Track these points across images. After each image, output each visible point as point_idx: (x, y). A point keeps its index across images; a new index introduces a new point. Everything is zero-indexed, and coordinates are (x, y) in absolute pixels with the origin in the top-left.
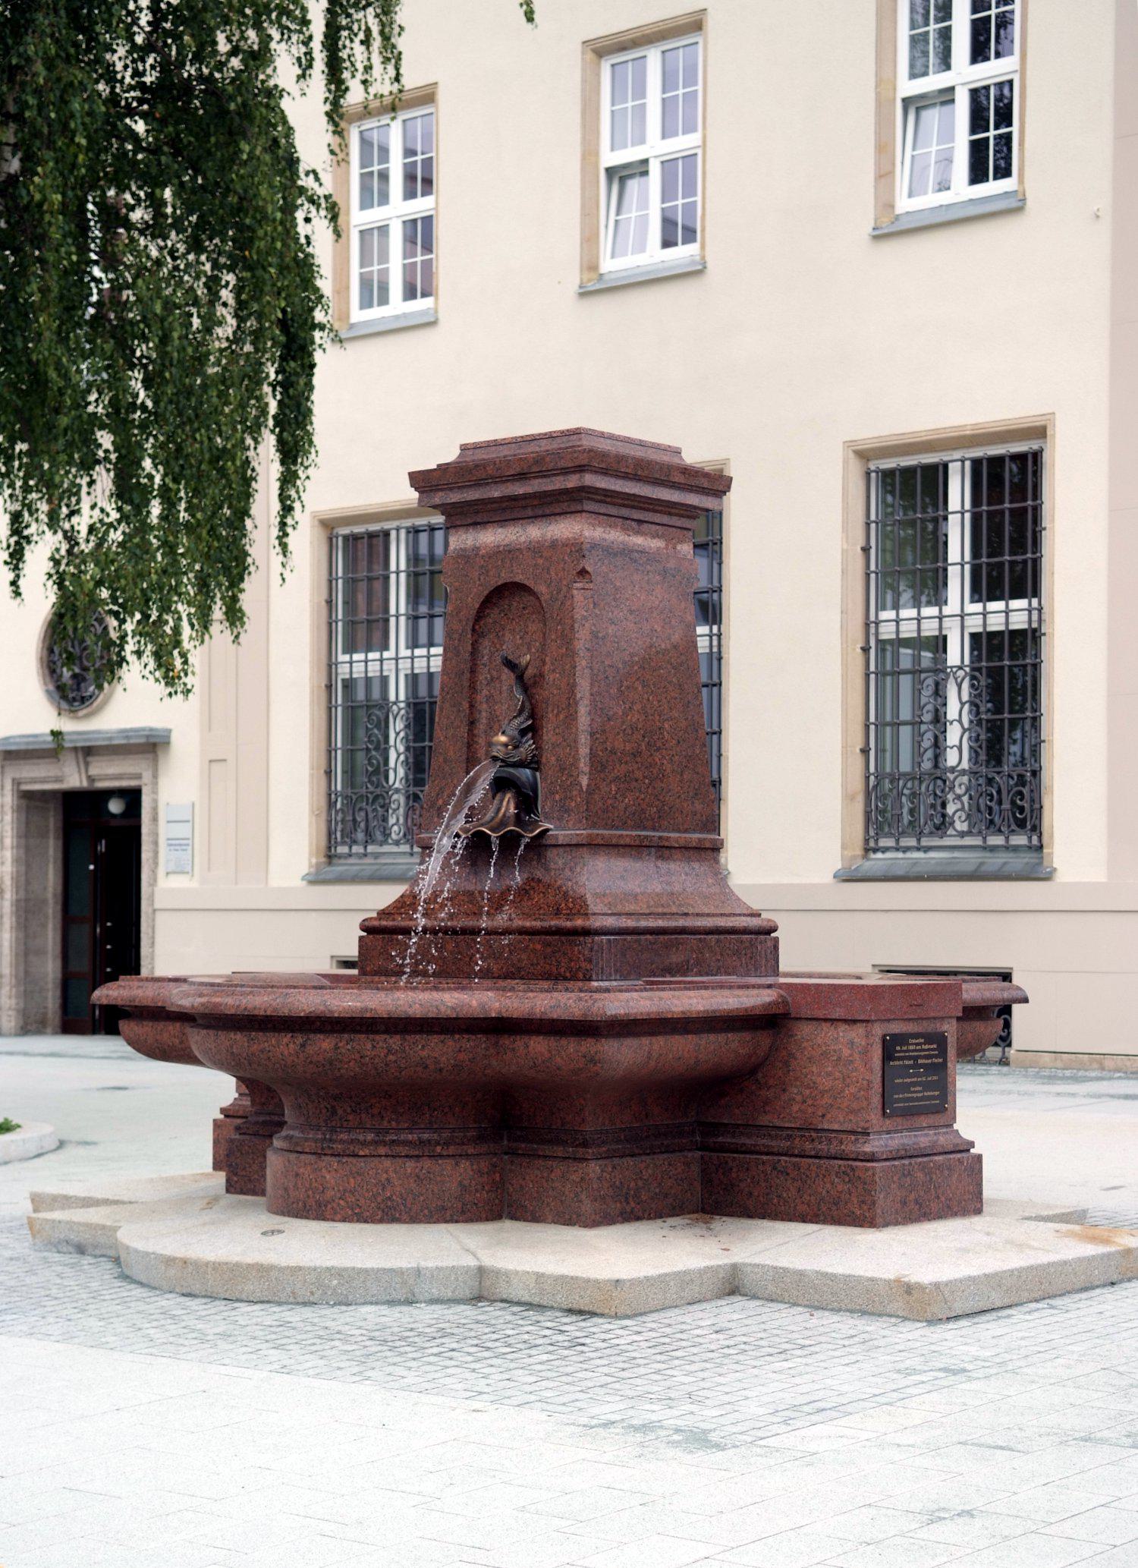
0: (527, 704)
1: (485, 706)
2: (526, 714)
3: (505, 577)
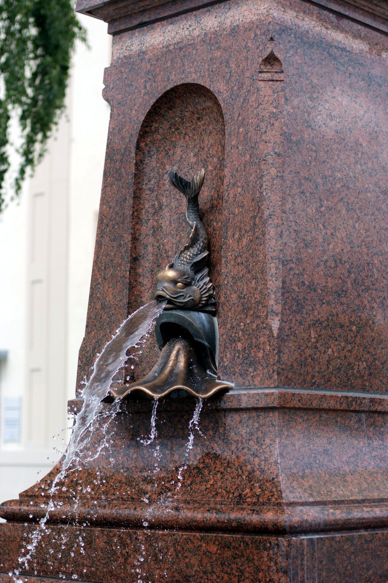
0: (202, 232)
1: (151, 239)
2: (200, 244)
3: (176, 79)
